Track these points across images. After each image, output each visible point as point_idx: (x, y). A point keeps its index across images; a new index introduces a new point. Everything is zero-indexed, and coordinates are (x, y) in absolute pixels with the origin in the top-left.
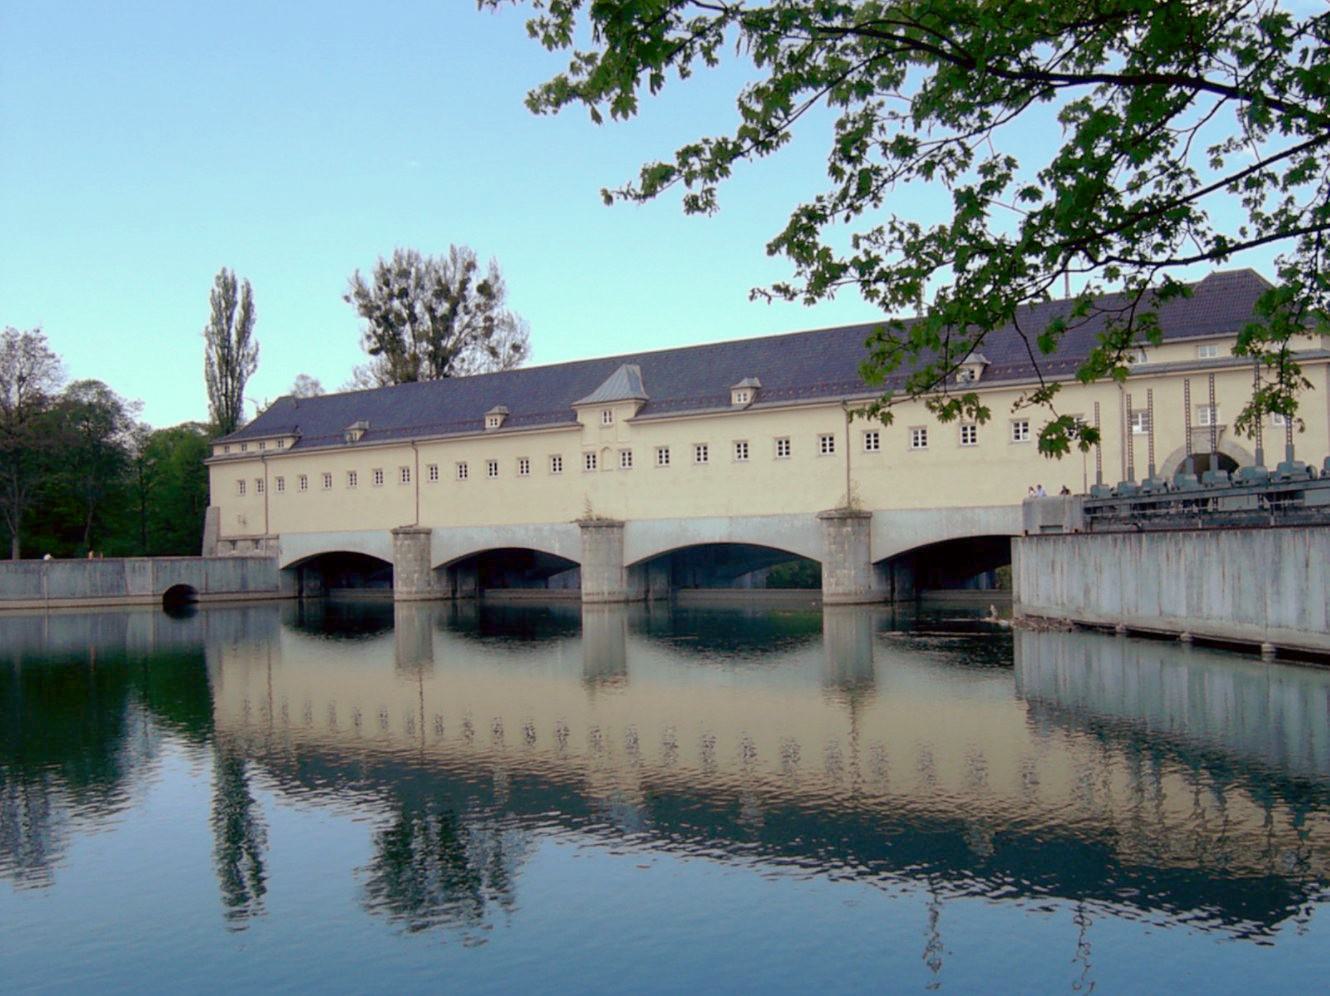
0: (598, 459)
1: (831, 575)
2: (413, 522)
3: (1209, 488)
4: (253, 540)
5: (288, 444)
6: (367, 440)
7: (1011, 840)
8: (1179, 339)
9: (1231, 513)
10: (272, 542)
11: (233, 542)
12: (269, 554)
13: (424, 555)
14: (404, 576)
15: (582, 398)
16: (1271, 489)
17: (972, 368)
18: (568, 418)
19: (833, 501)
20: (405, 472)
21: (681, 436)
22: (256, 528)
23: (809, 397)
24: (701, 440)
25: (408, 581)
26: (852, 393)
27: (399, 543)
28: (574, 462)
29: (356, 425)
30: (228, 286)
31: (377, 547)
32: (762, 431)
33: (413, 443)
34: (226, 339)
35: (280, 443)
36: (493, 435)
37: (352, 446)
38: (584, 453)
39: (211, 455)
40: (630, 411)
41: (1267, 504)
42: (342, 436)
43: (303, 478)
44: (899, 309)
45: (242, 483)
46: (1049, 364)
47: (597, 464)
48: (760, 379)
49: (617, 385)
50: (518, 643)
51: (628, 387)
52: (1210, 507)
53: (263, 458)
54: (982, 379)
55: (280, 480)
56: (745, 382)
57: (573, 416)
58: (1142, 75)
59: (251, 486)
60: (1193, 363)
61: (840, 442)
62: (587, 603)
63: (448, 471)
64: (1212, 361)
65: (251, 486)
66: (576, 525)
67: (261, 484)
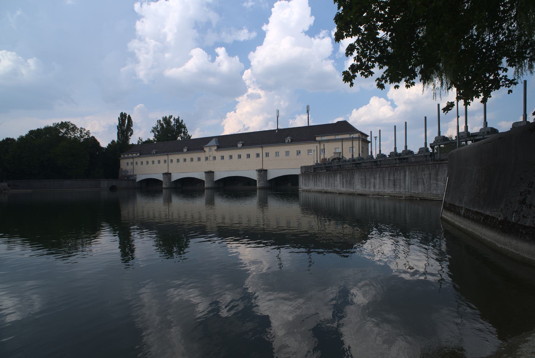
0: (208, 158)
5: (138, 154)
6: (243, 146)
7: (432, 246)
13: (170, 178)
15: (206, 145)
17: (289, 139)
18: (202, 149)
21: (226, 153)
24: (222, 155)
26: (263, 145)
29: (154, 151)
30: (123, 116)
32: (244, 152)
35: (137, 154)
36: (241, 148)
37: (154, 155)
38: (177, 159)
39: (121, 157)
40: (215, 148)
41: (354, 166)
42: (151, 153)
49: (213, 142)
50: (449, 212)
52: (342, 167)
53: (133, 158)
54: (291, 142)
56: (241, 142)
60: (349, 138)
61: (261, 155)
62: (303, 191)
63: (175, 161)
64: (324, 140)
65: (130, 164)
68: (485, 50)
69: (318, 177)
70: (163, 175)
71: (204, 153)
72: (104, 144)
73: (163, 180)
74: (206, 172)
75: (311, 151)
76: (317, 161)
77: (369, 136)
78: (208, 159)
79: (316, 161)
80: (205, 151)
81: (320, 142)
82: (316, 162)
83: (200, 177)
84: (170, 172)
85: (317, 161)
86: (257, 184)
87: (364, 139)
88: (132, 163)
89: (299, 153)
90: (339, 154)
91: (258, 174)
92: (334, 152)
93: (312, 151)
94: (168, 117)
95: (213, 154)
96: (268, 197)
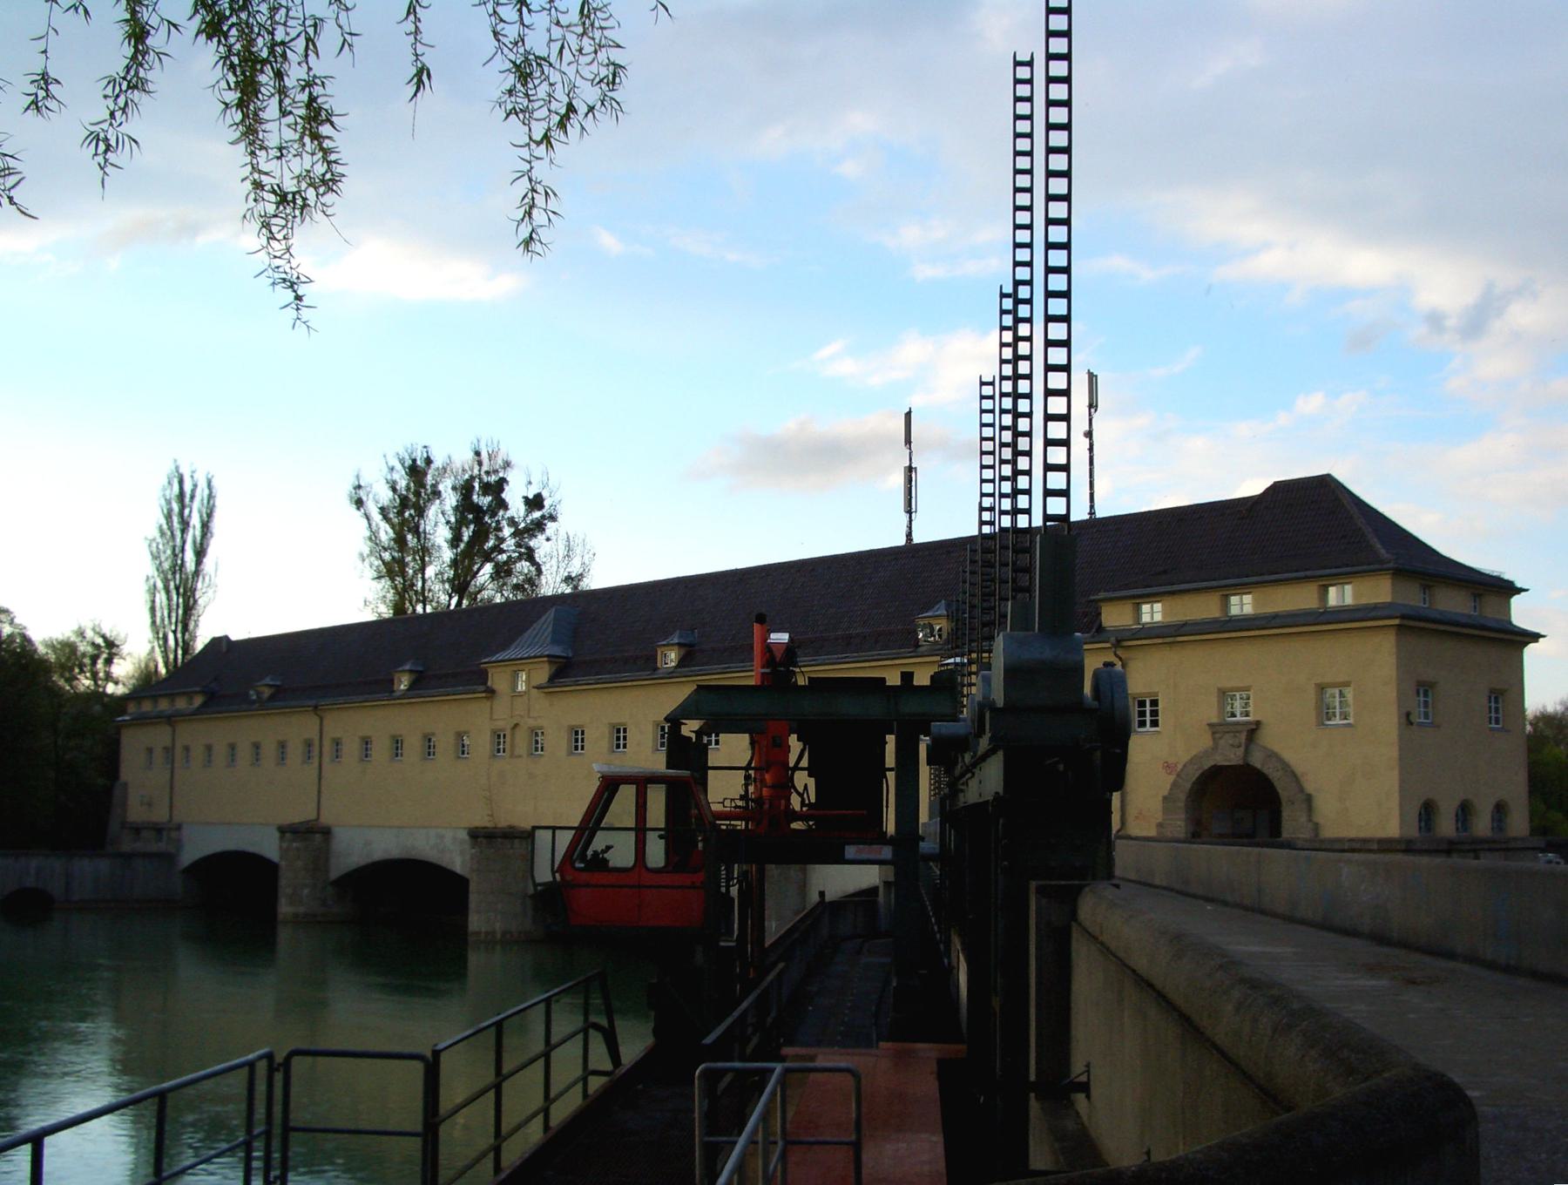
2: (313, 816)
5: (198, 701)
6: (684, 666)
8: (1162, 589)
14: (289, 891)
18: (473, 680)
28: (480, 743)
33: (316, 707)
34: (177, 553)
40: (543, 673)
44: (516, 516)
49: (541, 637)
57: (482, 677)
67: (169, 751)
70: (282, 838)
71: (489, 704)
72: (796, 736)
80: (491, 692)
84: (326, 819)
90: (1243, 737)
92: (1215, 720)
94: (388, 485)
95: (531, 715)
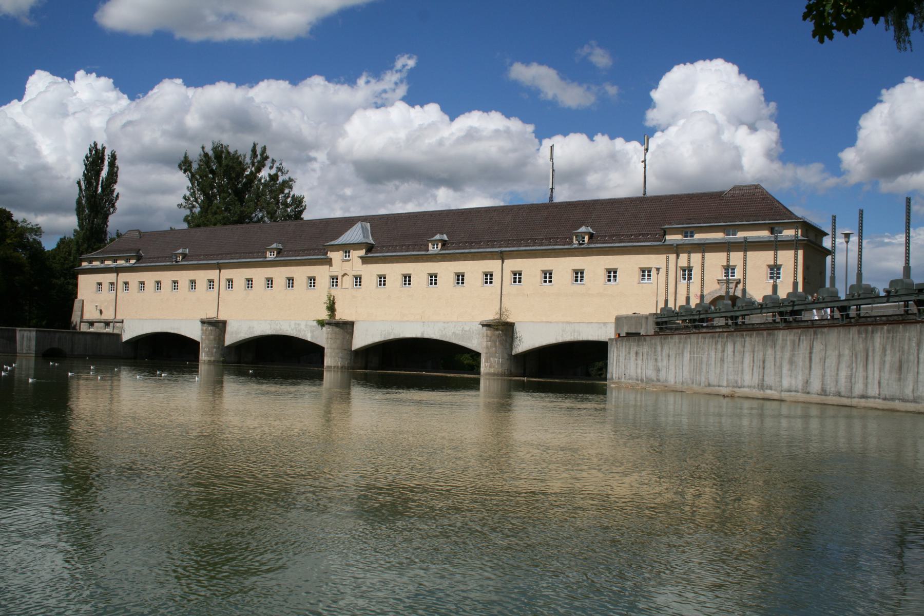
0: (339, 280)
1: (486, 361)
3: (741, 309)
4: (105, 322)
9: (753, 324)
10: (118, 325)
11: (91, 324)
12: (116, 331)
16: (782, 309)
19: (491, 315)
20: (211, 281)
22: (108, 315)
23: (478, 248)
25: (207, 355)
27: (204, 328)
31: (193, 331)
43: (142, 283)
45: (100, 284)
46: (632, 235)
47: (339, 284)
48: (447, 235)
49: (354, 234)
51: (362, 235)
52: (740, 321)
53: (118, 270)
55: (126, 283)
56: (438, 237)
58: (200, 213)
59: (106, 286)
61: (496, 278)
65: (106, 286)
66: (315, 322)
68: (836, 22)
69: (659, 348)
70: (202, 326)
73: (202, 338)
74: (203, 322)
75: (649, 271)
76: (666, 301)
77: (828, 235)
78: (339, 284)
79: (663, 302)
81: (677, 249)
82: (661, 305)
83: (312, 337)
85: (666, 301)
86: (482, 365)
87: (812, 242)
88: (112, 284)
89: (612, 274)
91: (487, 336)
93: (654, 272)
96: (226, 378)
